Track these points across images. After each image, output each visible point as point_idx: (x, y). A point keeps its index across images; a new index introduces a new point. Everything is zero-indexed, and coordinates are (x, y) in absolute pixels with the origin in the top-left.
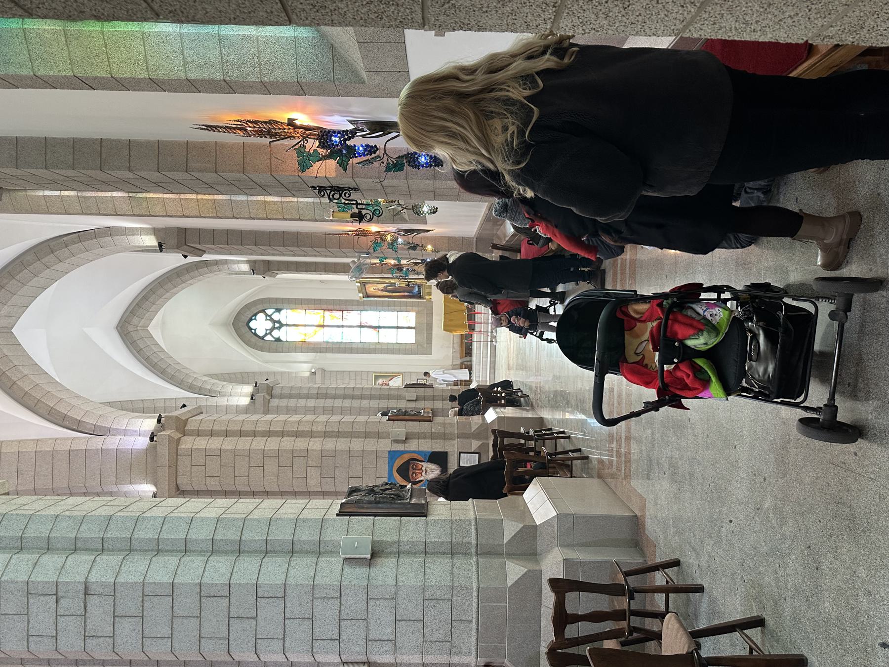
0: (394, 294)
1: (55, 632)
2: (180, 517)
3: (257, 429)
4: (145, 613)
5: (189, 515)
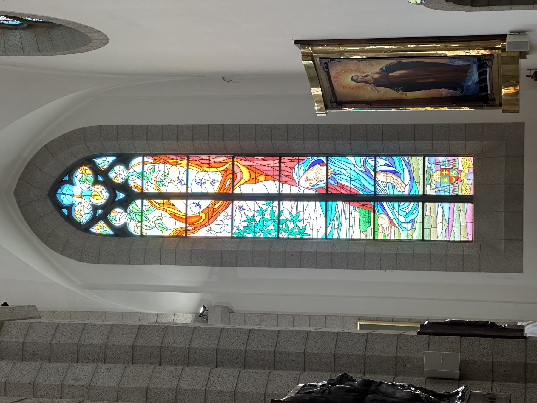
0: (411, 95)
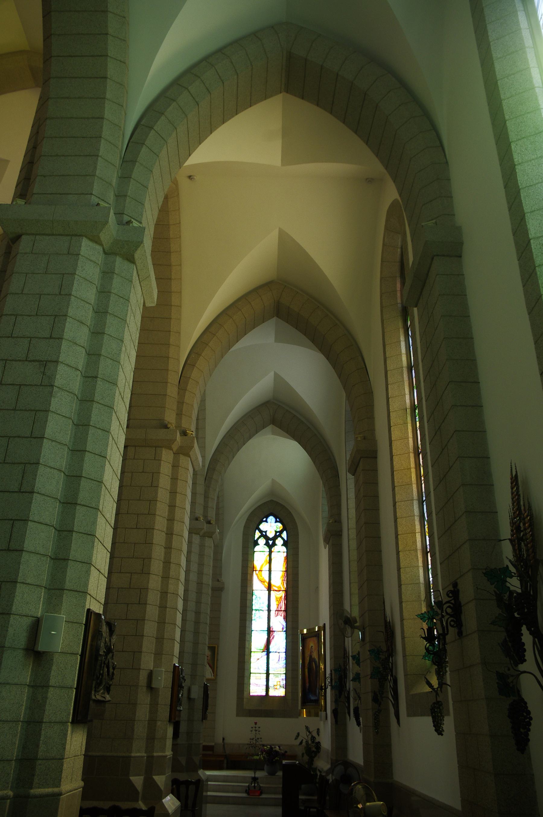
0: (306, 670)
1: (15, 336)
2: (107, 446)
3: (175, 522)
4: (19, 412)
5: (108, 454)
